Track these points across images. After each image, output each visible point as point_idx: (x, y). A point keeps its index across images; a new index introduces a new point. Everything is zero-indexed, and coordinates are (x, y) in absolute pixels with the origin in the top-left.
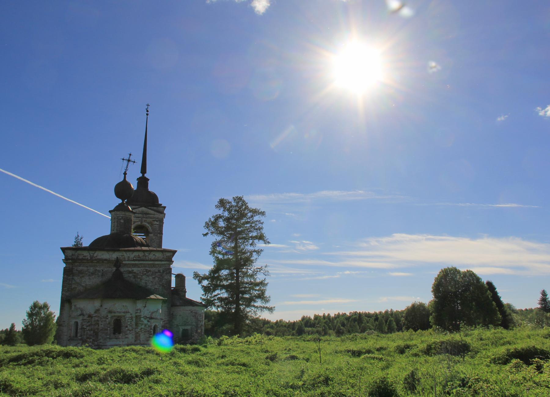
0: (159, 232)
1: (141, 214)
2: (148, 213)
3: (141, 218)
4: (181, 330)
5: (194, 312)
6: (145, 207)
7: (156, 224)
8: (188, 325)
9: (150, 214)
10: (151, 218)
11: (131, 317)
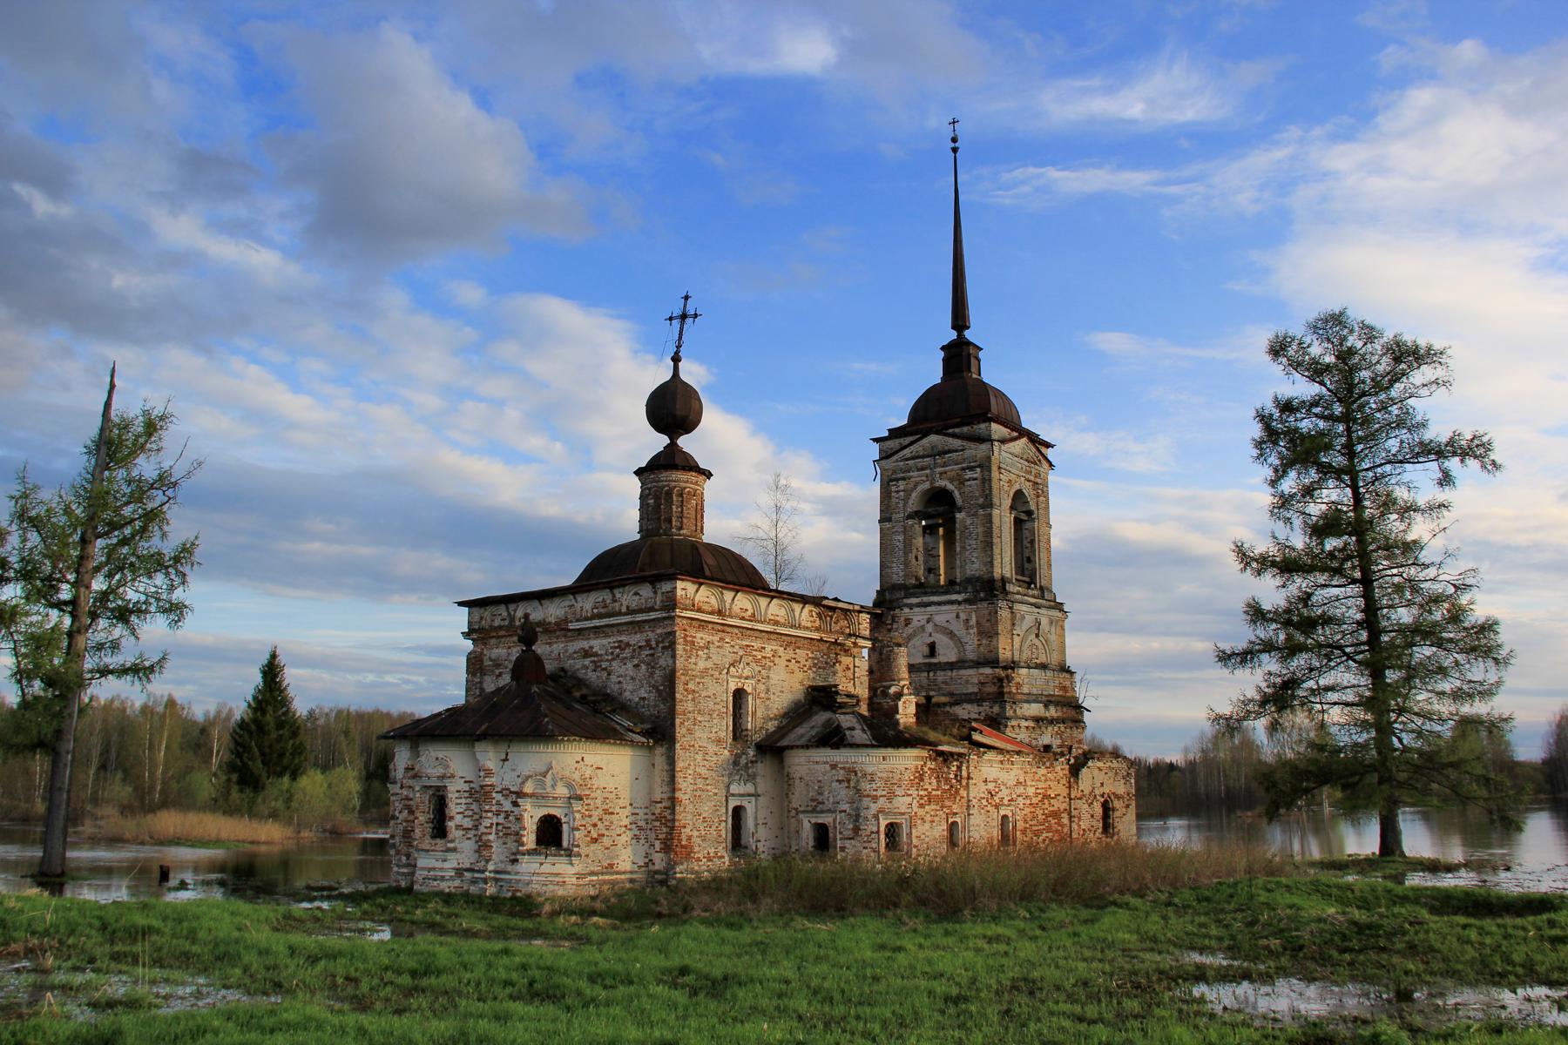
1: (928, 456)
2: (946, 448)
4: (807, 825)
5: (844, 768)
6: (938, 432)
9: (949, 451)
10: (957, 464)
11: (467, 789)
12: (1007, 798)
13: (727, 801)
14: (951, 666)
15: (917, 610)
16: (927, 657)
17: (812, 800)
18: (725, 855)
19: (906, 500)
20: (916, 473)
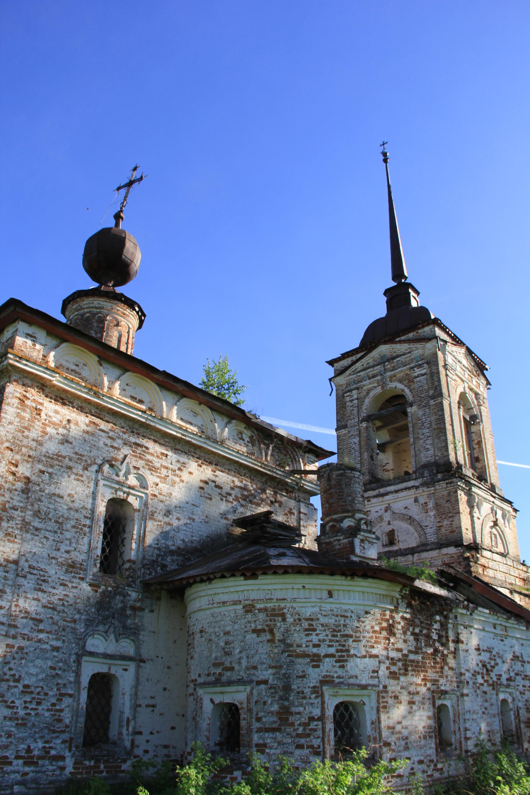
0: (431, 392)
2: (394, 354)
3: (381, 375)
4: (208, 707)
6: (385, 343)
7: (418, 376)
8: (230, 683)
9: (398, 356)
10: (405, 365)
12: (505, 676)
13: (79, 662)
14: (412, 551)
15: (374, 500)
16: (386, 545)
17: (216, 665)
18: (67, 754)
19: (359, 407)
20: (368, 382)
